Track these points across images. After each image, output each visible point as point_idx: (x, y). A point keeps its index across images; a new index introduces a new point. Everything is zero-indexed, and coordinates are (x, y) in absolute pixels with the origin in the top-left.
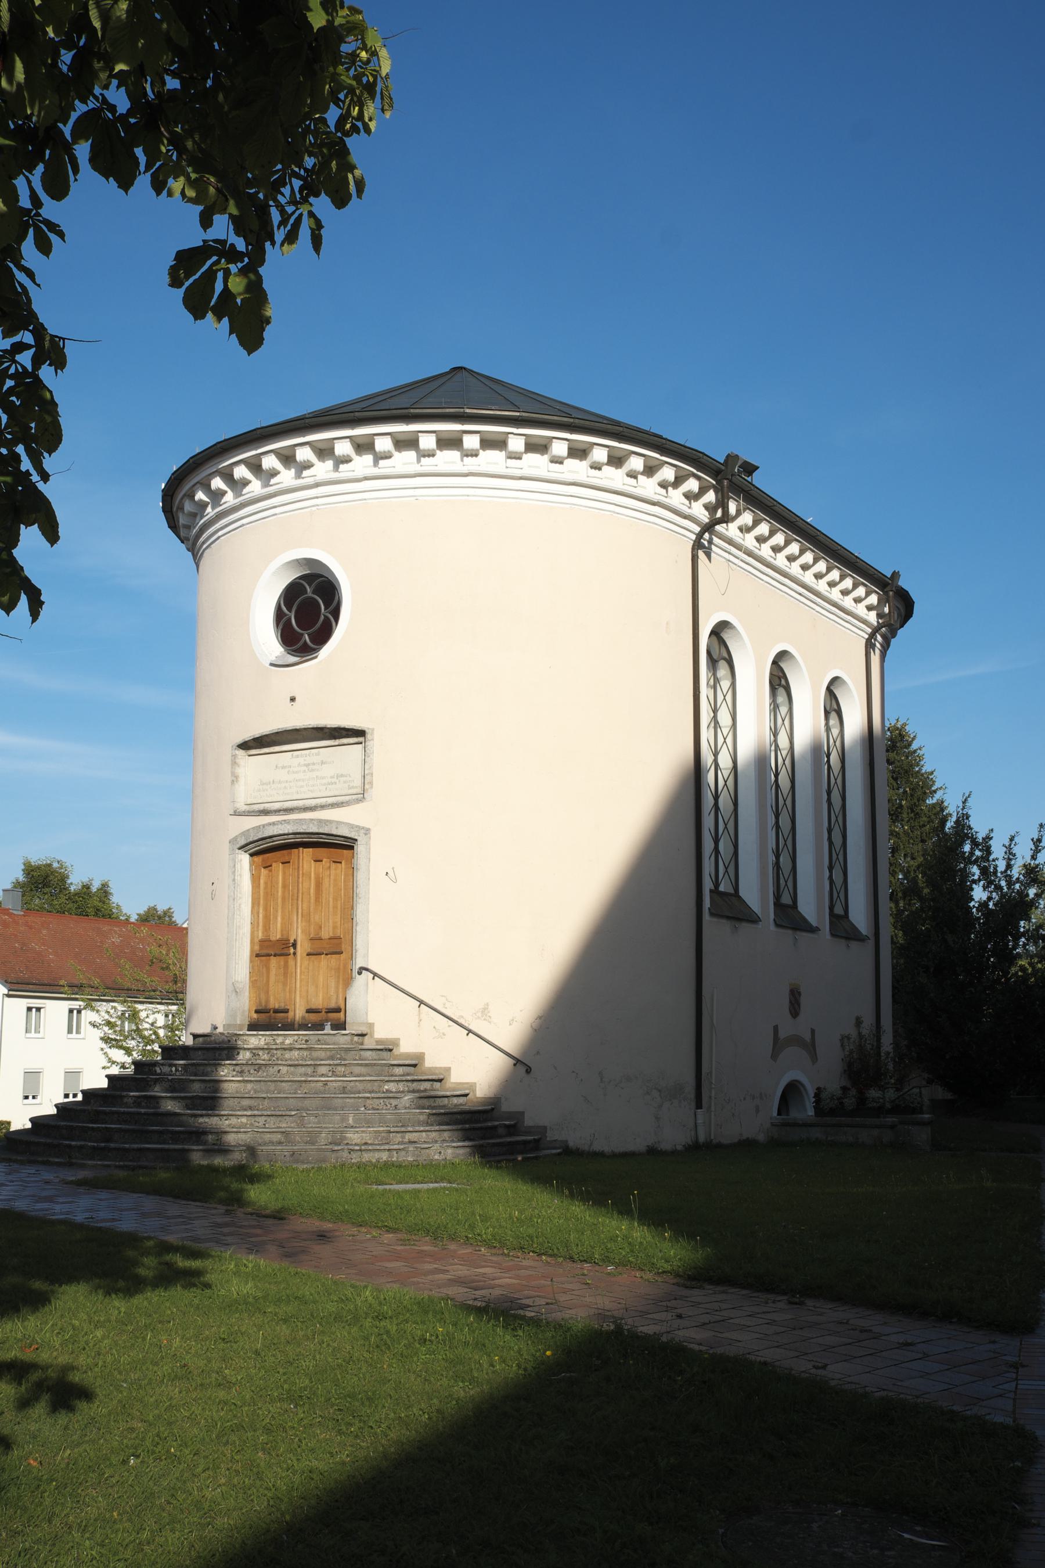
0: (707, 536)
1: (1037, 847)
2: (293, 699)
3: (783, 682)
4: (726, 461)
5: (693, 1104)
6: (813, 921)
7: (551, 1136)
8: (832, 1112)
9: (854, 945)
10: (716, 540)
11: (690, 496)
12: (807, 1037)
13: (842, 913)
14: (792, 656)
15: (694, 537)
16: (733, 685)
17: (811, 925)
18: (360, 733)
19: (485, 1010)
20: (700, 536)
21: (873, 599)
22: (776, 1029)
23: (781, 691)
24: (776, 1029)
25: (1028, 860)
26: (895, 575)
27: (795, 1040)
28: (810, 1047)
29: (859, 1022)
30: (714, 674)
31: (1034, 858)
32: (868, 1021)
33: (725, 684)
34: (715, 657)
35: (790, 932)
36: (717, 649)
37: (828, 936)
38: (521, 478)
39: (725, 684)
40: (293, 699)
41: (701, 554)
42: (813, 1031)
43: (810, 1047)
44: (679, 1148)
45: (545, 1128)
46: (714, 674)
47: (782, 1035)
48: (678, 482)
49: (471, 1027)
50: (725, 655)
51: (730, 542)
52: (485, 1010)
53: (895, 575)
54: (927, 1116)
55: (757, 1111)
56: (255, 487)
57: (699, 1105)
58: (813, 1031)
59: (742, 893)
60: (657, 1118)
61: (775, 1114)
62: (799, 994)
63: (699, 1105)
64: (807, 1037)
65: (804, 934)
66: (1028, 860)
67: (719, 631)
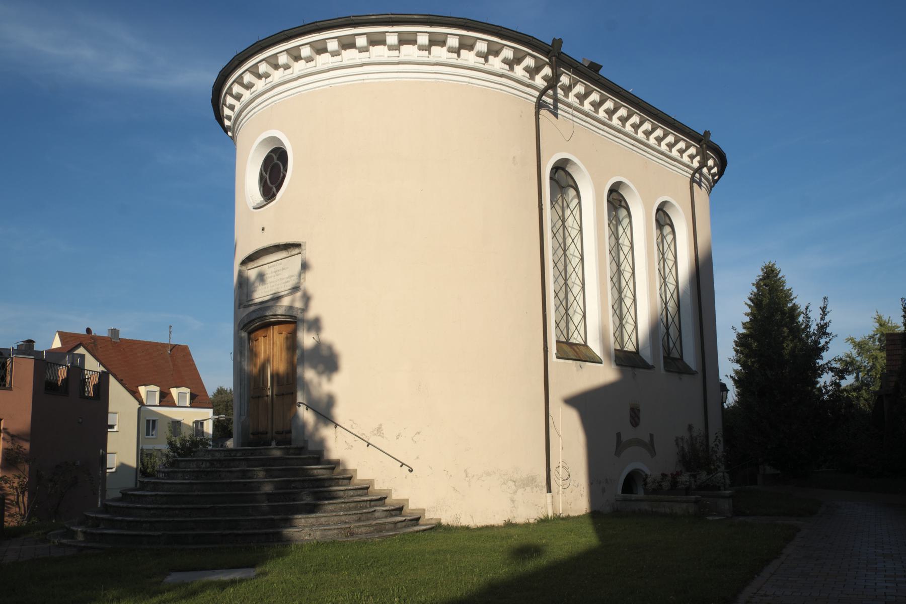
0: (697, 175)
1: (824, 312)
2: (263, 229)
3: (623, 203)
4: (553, 43)
5: (545, 490)
6: (650, 361)
7: (427, 516)
8: (655, 491)
9: (685, 377)
10: (560, 105)
11: (510, 64)
12: (647, 439)
13: (678, 357)
14: (628, 186)
15: (535, 100)
16: (674, 238)
17: (690, 369)
18: (298, 246)
19: (379, 429)
20: (693, 175)
21: (692, 150)
22: (619, 435)
23: (667, 229)
24: (619, 435)
25: (819, 321)
26: (707, 133)
27: (638, 442)
28: (650, 447)
29: (690, 428)
30: (662, 233)
31: (822, 319)
32: (698, 427)
33: (669, 238)
34: (662, 223)
35: (630, 369)
36: (562, 177)
37: (663, 371)
38: (399, 63)
39: (669, 238)
40: (263, 229)
41: (695, 185)
42: (651, 436)
43: (650, 447)
44: (532, 521)
45: (424, 510)
46: (662, 233)
47: (624, 438)
48: (517, 60)
49: (370, 442)
50: (668, 222)
51: (569, 106)
52: (379, 429)
53: (707, 133)
54: (728, 492)
55: (604, 490)
56: (247, 95)
57: (549, 490)
58: (651, 436)
59: (588, 344)
60: (513, 501)
61: (619, 492)
62: (639, 410)
63: (549, 490)
64: (647, 439)
65: (641, 370)
66: (819, 321)
67: (561, 167)
